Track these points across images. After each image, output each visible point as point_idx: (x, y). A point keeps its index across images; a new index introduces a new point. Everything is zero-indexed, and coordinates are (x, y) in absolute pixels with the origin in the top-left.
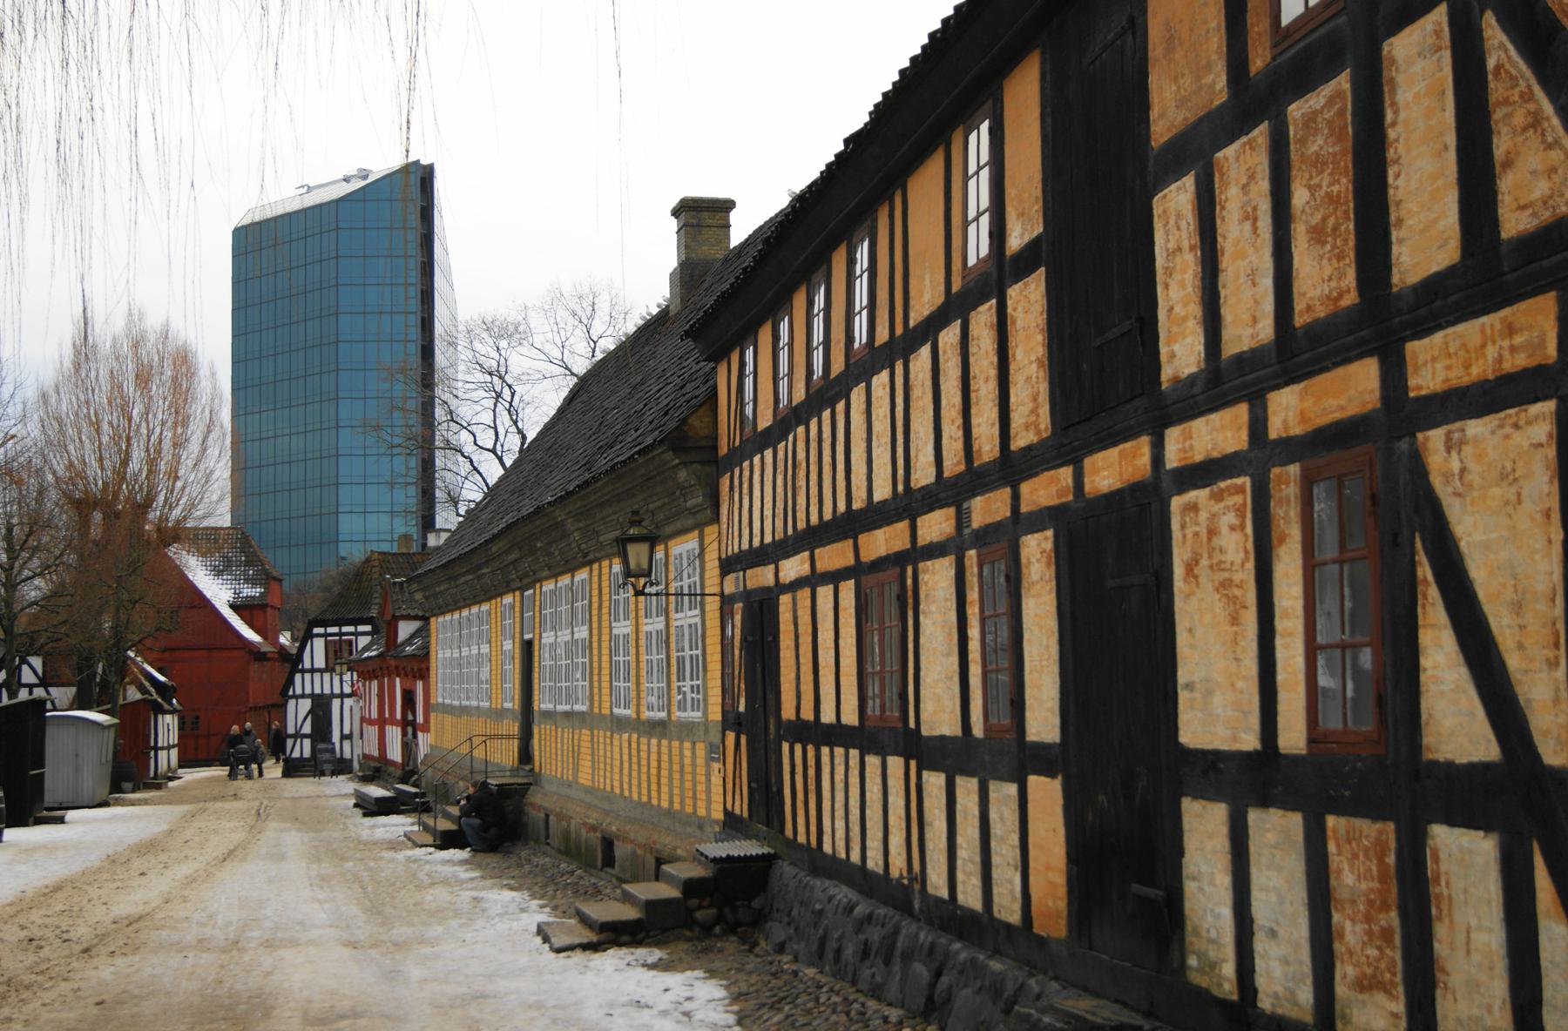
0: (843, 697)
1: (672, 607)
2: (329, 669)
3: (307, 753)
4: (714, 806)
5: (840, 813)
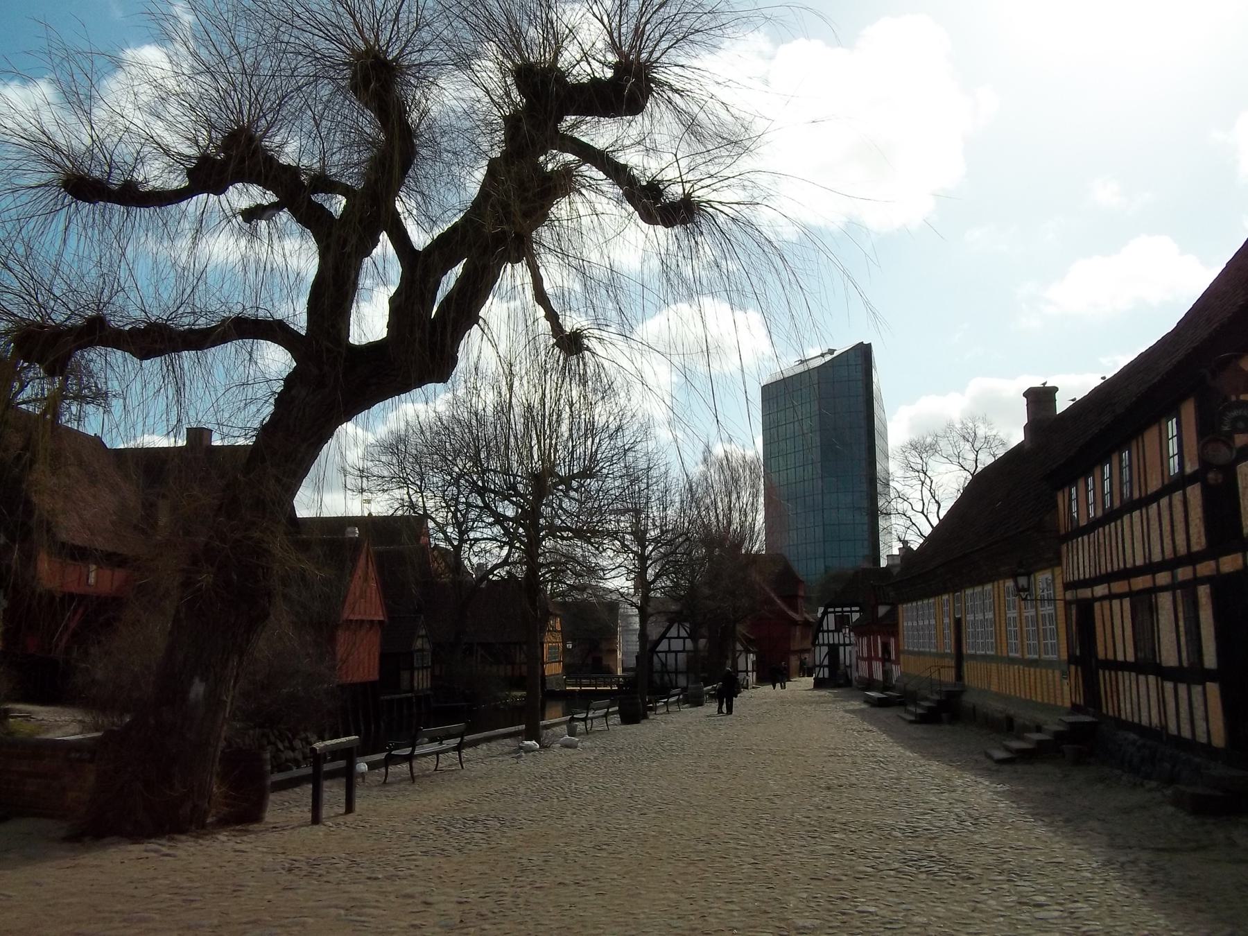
2: (838, 630)
3: (826, 675)
5: (1128, 701)
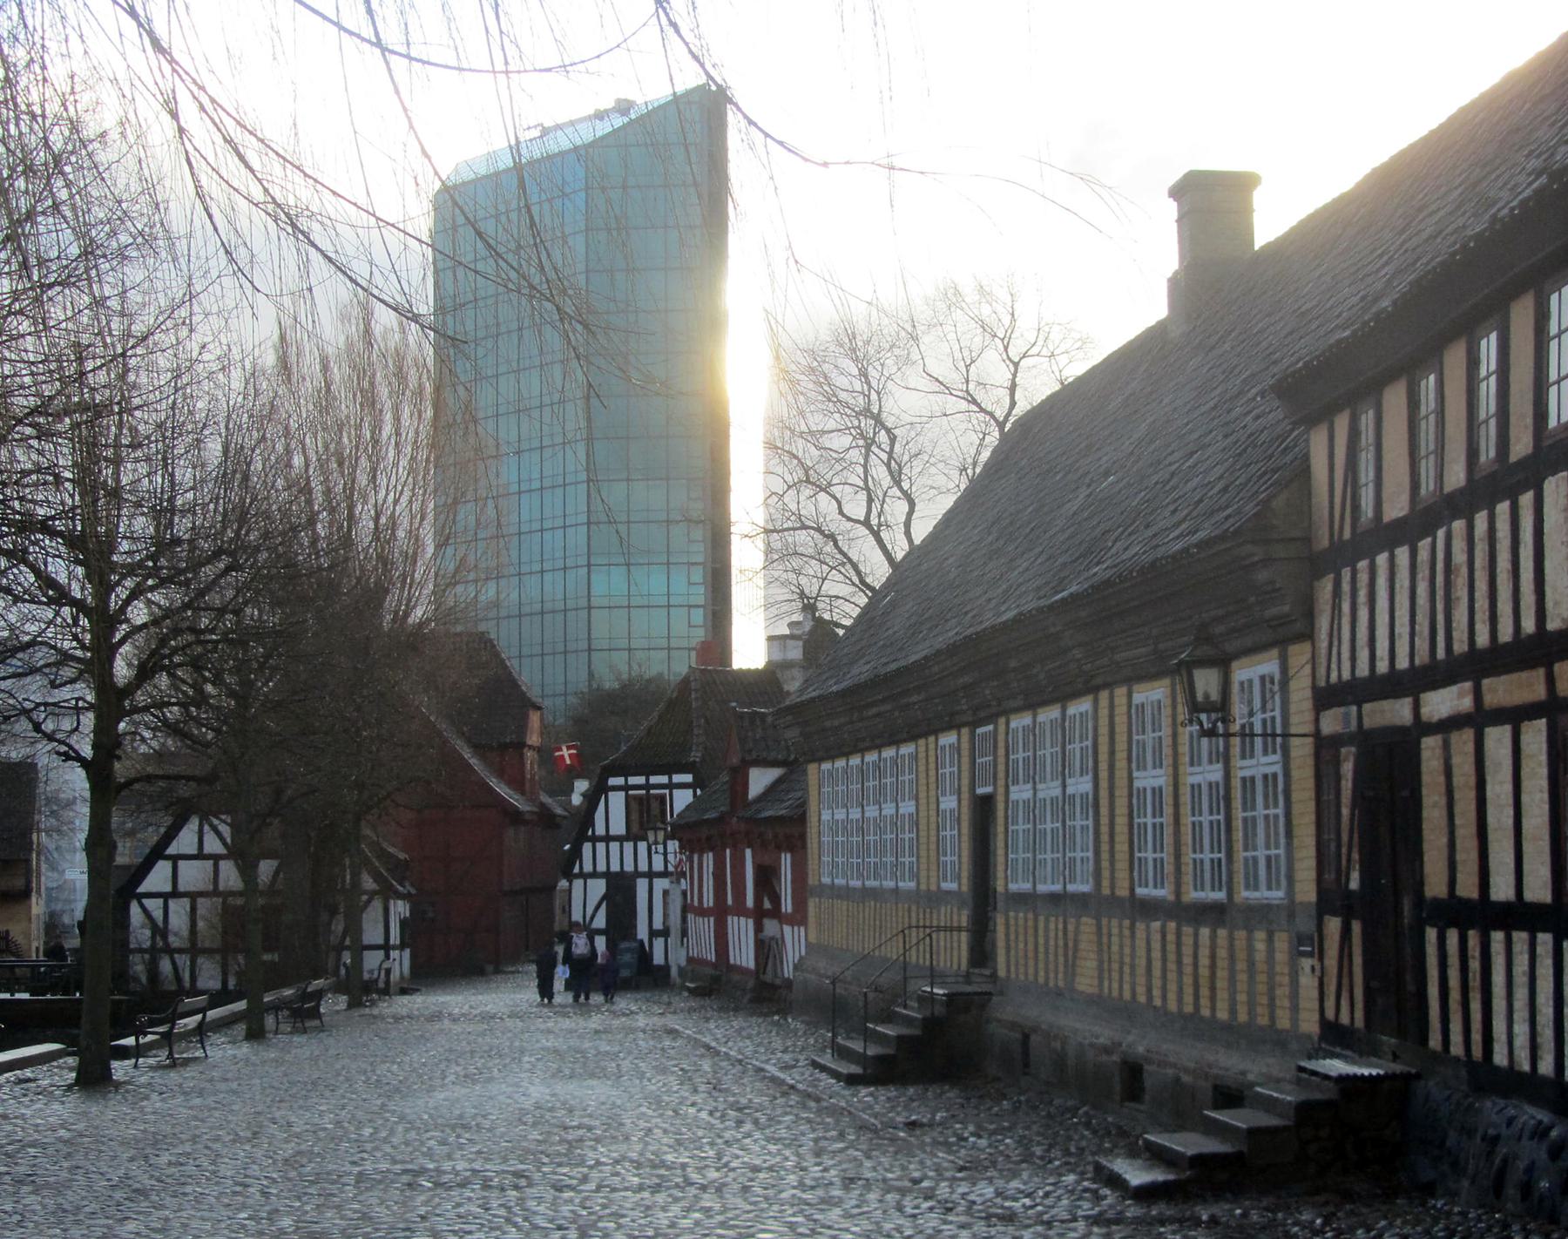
0: (1526, 867)
1: (1236, 749)
2: (633, 835)
4: (1303, 1015)
5: (1521, 1013)
